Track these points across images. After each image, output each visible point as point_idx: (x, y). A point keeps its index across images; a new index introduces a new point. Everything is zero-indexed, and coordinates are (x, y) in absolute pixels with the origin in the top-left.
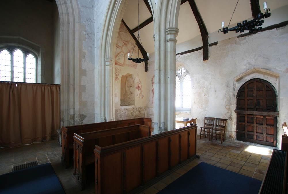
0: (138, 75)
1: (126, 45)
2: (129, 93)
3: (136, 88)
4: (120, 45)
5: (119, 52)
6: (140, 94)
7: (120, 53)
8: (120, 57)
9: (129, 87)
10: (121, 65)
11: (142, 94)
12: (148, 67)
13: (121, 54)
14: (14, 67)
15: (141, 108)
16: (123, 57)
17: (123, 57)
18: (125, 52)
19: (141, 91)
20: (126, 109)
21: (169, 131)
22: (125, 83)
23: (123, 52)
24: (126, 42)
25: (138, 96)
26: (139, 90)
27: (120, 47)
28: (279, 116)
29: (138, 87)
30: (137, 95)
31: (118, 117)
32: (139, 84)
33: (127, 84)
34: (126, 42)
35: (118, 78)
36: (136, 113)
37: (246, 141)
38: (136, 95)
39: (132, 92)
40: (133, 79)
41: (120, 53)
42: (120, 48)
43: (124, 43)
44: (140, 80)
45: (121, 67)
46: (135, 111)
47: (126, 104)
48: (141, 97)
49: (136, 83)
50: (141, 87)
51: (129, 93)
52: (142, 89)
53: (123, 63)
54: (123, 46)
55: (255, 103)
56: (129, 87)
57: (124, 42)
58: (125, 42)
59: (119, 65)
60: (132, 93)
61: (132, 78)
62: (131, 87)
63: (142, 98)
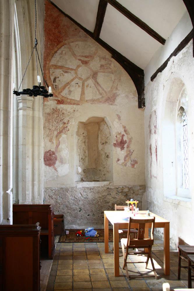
0: (119, 118)
1: (85, 63)
2: (103, 156)
3: (115, 145)
4: (70, 67)
5: (69, 81)
6: (126, 156)
7: (72, 80)
8: (72, 89)
9: (103, 144)
10: (74, 104)
11: (133, 157)
12: (144, 99)
13: (73, 83)
14: (16, 145)
15: (130, 189)
16: (79, 86)
17: (79, 86)
18: (84, 77)
19: (130, 151)
20: (88, 188)
21: (20, 205)
22: (98, 136)
23: (80, 79)
24: (86, 57)
25: (122, 161)
26: (122, 148)
27: (72, 69)
28: (30, 96)
29: (121, 144)
30: (118, 160)
31: (69, 202)
32: (123, 135)
33: (100, 139)
34: (86, 57)
35: (69, 127)
36: (115, 198)
37: (103, 218)
38: (115, 160)
39: (107, 154)
40: (108, 128)
41: (72, 80)
42: (73, 72)
43: (80, 62)
44: (125, 127)
45: (75, 106)
46: (113, 194)
47: (96, 178)
48: (129, 164)
49: (114, 133)
50: (128, 142)
51: (103, 156)
52: (132, 147)
53: (79, 99)
54: (78, 66)
55: (116, 93)
56: (103, 144)
57: (79, 60)
58: (82, 59)
59: (70, 103)
60: (108, 156)
61: (107, 126)
62: (106, 142)
63: (133, 165)
